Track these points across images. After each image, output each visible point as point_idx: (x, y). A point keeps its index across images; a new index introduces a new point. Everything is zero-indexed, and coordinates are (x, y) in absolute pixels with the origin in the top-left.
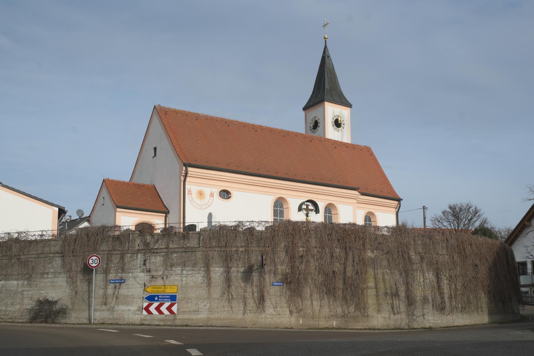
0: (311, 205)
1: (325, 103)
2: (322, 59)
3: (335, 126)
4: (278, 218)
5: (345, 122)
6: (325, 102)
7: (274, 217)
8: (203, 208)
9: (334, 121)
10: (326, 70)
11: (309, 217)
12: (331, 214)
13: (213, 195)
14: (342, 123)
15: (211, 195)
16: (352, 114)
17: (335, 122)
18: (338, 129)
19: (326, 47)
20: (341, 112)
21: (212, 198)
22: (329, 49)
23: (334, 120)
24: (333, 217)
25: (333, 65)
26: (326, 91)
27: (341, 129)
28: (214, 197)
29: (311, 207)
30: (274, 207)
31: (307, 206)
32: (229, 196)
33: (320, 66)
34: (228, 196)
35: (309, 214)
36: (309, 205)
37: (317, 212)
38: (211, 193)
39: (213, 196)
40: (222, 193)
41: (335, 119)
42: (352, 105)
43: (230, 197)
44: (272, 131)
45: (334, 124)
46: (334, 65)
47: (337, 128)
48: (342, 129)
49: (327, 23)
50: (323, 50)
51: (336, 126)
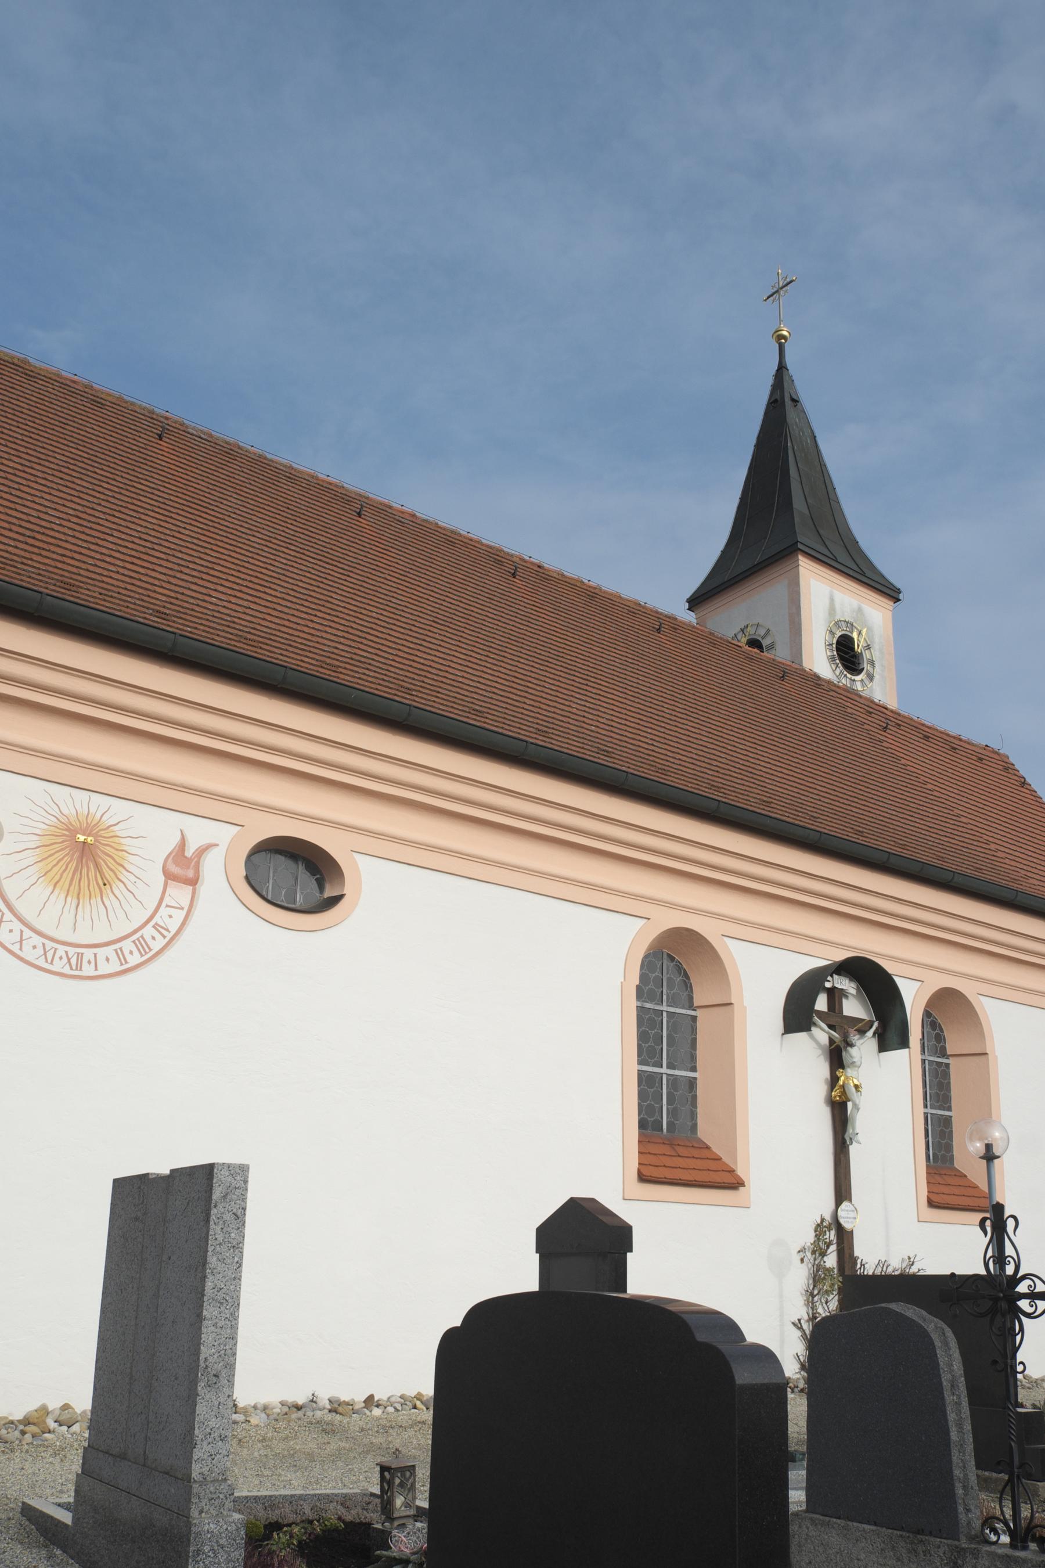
0: (858, 996)
1: (800, 563)
2: (766, 413)
3: (840, 665)
4: (664, 1070)
5: (876, 654)
6: (800, 557)
7: (640, 1063)
8: (88, 970)
9: (835, 641)
10: (789, 444)
11: (849, 1072)
12: (943, 1053)
13: (190, 874)
14: (867, 655)
15: (174, 869)
16: (899, 627)
17: (838, 650)
18: (853, 678)
19: (782, 368)
20: (860, 610)
21: (180, 894)
22: (794, 378)
23: (837, 636)
24: (952, 1070)
25: (815, 437)
26: (797, 519)
27: (862, 680)
28: (204, 889)
29: (853, 1008)
30: (641, 993)
31: (835, 996)
32: (329, 892)
33: (759, 437)
34: (321, 888)
35: (853, 1051)
36: (843, 993)
37: (892, 1036)
38: (179, 854)
39: (193, 882)
40: (256, 858)
41: (838, 634)
42: (899, 591)
43: (334, 901)
44: (592, 596)
45: (835, 653)
46: (817, 434)
47: (849, 676)
48: (867, 681)
49: (788, 280)
50: (770, 380)
51: (843, 665)
